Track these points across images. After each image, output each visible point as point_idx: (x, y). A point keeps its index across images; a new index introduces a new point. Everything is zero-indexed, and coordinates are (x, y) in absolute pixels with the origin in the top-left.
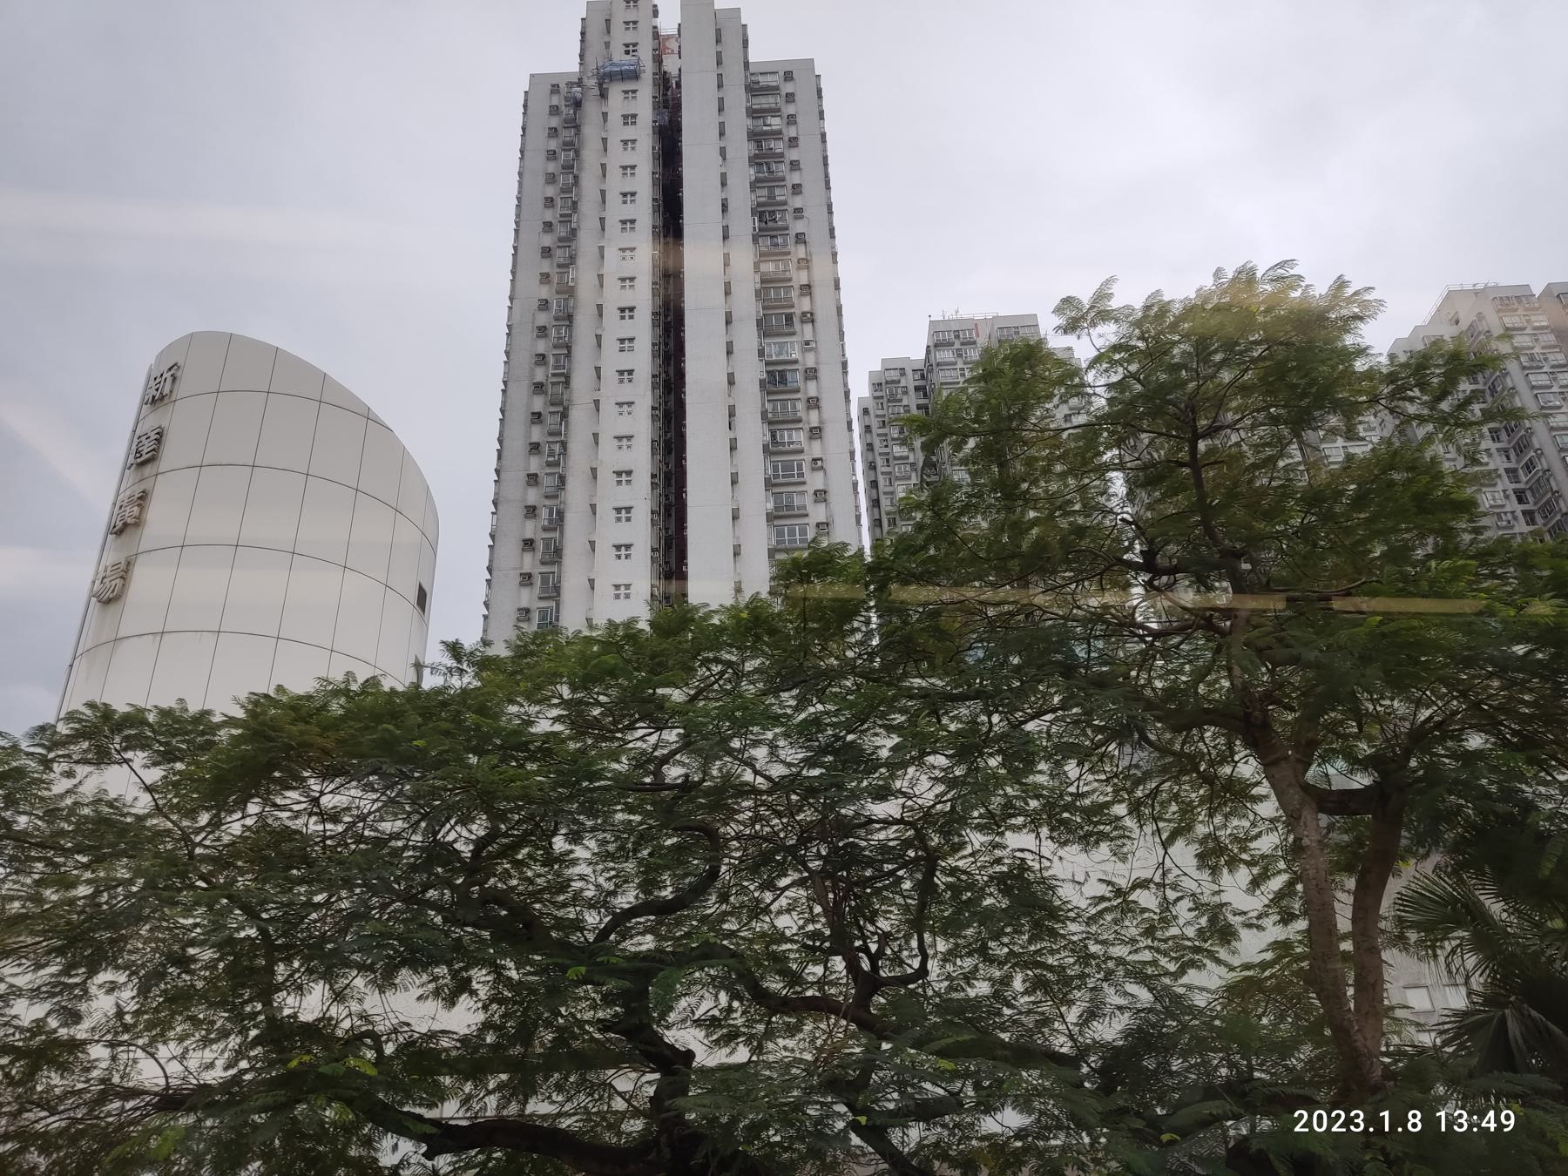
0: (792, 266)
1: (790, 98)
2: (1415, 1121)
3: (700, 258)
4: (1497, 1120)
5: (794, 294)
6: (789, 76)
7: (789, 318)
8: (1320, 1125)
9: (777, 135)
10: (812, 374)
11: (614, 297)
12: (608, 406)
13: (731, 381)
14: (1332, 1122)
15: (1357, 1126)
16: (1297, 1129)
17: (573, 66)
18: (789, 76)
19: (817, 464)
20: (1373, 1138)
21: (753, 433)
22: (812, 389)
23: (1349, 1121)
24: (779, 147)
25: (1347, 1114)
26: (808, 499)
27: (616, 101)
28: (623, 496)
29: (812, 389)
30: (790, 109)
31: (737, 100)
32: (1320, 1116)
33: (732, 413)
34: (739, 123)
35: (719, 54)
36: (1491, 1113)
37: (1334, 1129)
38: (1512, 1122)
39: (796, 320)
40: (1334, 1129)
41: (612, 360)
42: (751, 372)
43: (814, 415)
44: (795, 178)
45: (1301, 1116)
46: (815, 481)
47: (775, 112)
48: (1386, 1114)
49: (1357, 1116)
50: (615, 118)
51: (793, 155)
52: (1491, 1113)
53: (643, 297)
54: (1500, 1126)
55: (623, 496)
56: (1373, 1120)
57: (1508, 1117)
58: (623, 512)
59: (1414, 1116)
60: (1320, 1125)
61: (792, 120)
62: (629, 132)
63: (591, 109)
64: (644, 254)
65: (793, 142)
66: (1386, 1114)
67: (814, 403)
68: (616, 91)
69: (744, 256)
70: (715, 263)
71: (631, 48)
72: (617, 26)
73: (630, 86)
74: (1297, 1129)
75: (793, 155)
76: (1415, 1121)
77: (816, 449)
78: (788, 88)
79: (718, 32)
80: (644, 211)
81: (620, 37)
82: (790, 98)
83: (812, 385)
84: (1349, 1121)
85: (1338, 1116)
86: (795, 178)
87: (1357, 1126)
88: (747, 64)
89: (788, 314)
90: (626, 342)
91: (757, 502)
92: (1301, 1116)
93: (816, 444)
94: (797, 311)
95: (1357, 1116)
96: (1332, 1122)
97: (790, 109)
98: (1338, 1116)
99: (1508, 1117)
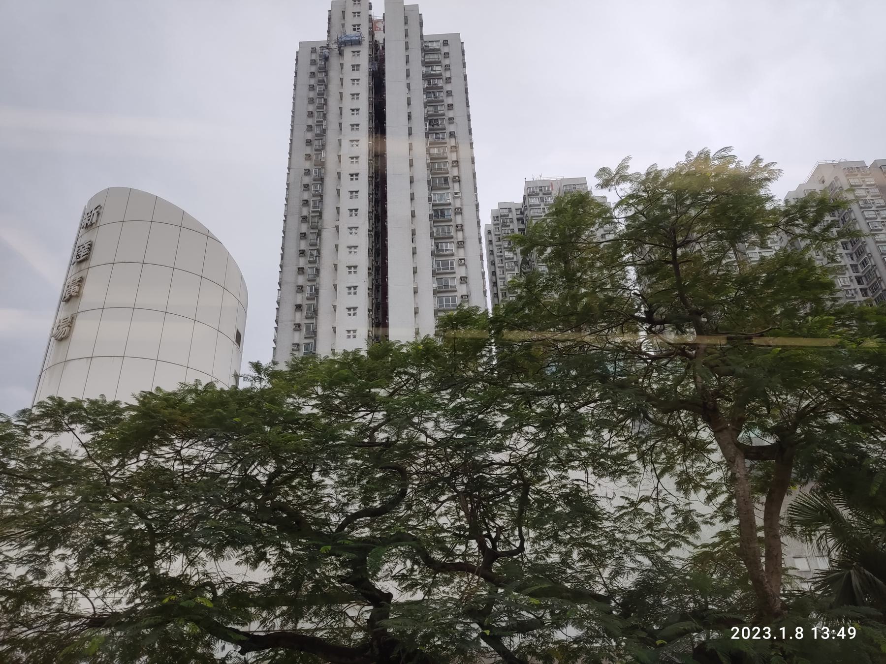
0: (448, 150)
1: (446, 55)
2: (799, 633)
3: (396, 146)
4: (846, 632)
5: (449, 166)
6: (446, 43)
7: (446, 179)
8: (746, 635)
9: (439, 76)
10: (459, 211)
11: (347, 167)
12: (343, 230)
13: (413, 215)
14: (753, 633)
15: (767, 635)
16: (733, 638)
17: (324, 37)
18: (446, 43)
19: (462, 262)
20: (776, 643)
21: (425, 245)
22: (459, 220)
23: (762, 633)
24: (440, 83)
25: (761, 629)
26: (457, 282)
27: (348, 57)
28: (352, 280)
29: (459, 220)
30: (446, 62)
31: (417, 56)
32: (746, 630)
33: (413, 233)
34: (417, 70)
35: (406, 31)
36: (843, 629)
37: (754, 638)
38: (854, 633)
39: (450, 181)
40: (754, 638)
41: (346, 203)
42: (424, 210)
43: (460, 234)
44: (449, 100)
45: (735, 630)
46: (460, 272)
47: (438, 63)
48: (783, 629)
49: (767, 630)
50: (348, 67)
51: (448, 87)
52: (843, 629)
53: (363, 168)
54: (848, 636)
55: (352, 280)
56: (776, 632)
57: (852, 631)
58: (352, 289)
59: (799, 630)
60: (746, 635)
61: (447, 68)
62: (355, 75)
63: (334, 62)
64: (364, 144)
65: (448, 80)
66: (783, 629)
67: (460, 228)
68: (348, 51)
69: (420, 145)
70: (404, 149)
71: (356, 27)
72: (349, 15)
73: (356, 49)
74: (733, 638)
75: (448, 87)
76: (799, 633)
77: (461, 254)
78: (445, 50)
79: (406, 18)
80: (364, 119)
81: (350, 21)
82: (446, 55)
83: (459, 217)
84: (762, 633)
85: (756, 630)
86: (449, 100)
87: (767, 635)
88: (422, 36)
89: (446, 178)
90: (354, 193)
91: (428, 283)
92: (735, 630)
93: (461, 251)
94: (450, 176)
95: (767, 630)
96: (753, 633)
97: (446, 62)
98: (756, 630)
99: (852, 631)
